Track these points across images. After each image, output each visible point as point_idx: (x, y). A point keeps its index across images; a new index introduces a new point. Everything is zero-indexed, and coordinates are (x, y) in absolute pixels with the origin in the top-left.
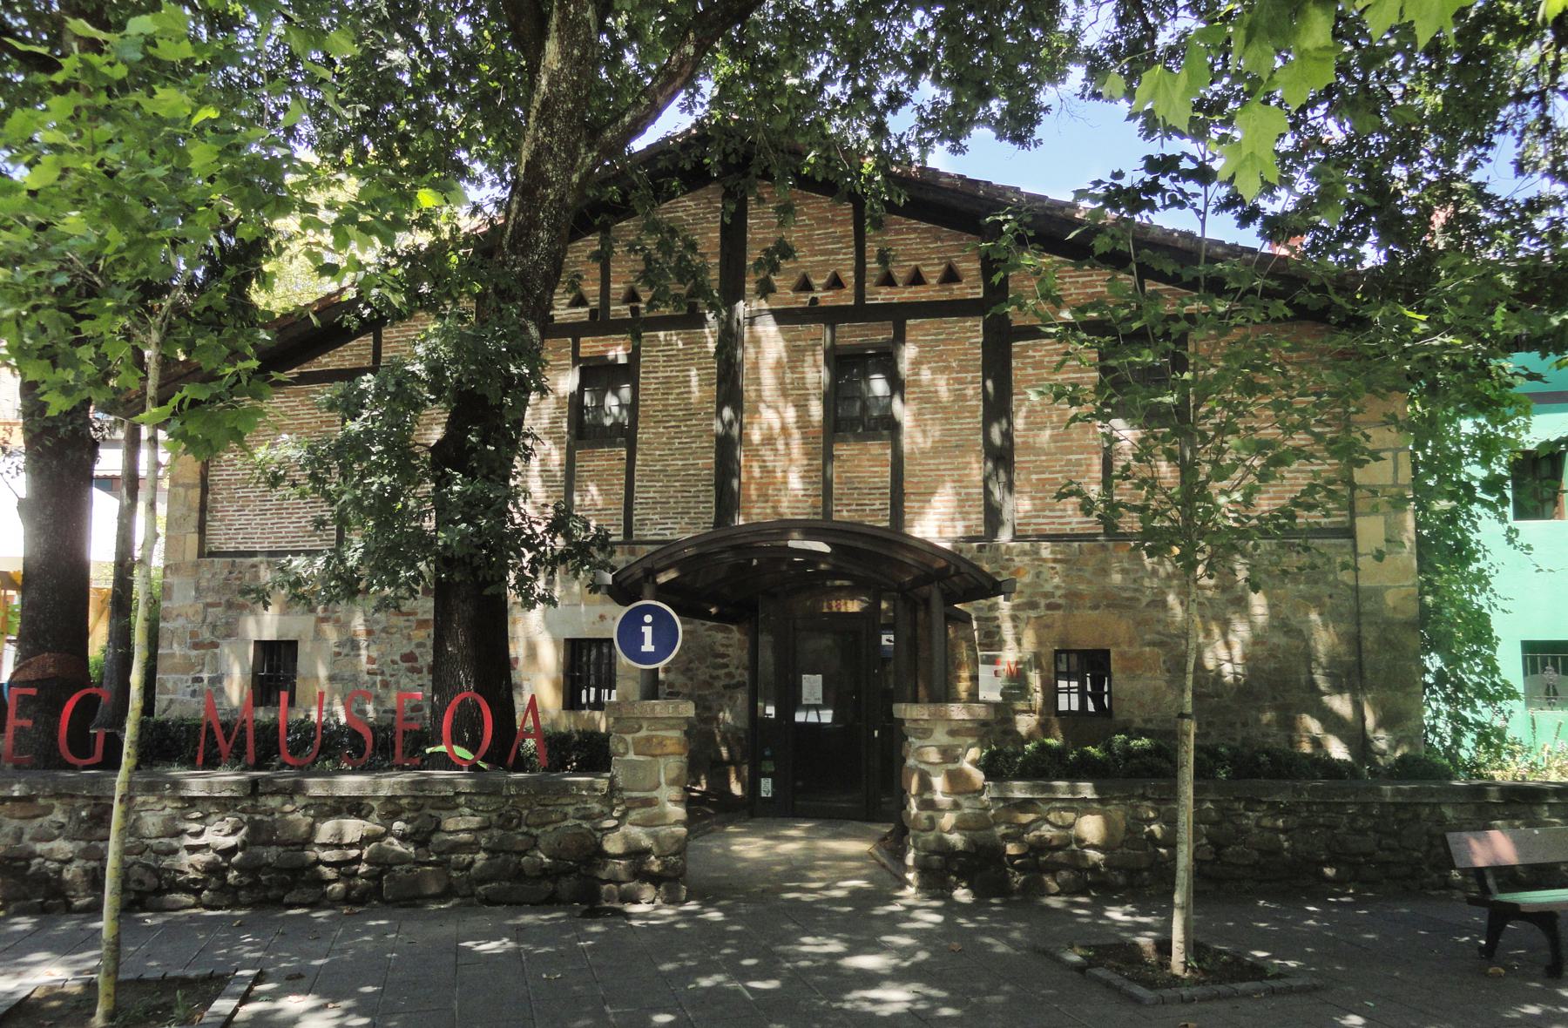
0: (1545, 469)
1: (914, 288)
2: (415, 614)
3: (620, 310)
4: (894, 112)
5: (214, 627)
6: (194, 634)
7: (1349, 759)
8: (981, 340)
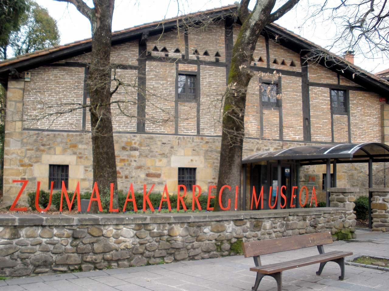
0: (193, 171)
3: (192, 57)
5: (30, 158)
6: (21, 161)
8: (301, 84)
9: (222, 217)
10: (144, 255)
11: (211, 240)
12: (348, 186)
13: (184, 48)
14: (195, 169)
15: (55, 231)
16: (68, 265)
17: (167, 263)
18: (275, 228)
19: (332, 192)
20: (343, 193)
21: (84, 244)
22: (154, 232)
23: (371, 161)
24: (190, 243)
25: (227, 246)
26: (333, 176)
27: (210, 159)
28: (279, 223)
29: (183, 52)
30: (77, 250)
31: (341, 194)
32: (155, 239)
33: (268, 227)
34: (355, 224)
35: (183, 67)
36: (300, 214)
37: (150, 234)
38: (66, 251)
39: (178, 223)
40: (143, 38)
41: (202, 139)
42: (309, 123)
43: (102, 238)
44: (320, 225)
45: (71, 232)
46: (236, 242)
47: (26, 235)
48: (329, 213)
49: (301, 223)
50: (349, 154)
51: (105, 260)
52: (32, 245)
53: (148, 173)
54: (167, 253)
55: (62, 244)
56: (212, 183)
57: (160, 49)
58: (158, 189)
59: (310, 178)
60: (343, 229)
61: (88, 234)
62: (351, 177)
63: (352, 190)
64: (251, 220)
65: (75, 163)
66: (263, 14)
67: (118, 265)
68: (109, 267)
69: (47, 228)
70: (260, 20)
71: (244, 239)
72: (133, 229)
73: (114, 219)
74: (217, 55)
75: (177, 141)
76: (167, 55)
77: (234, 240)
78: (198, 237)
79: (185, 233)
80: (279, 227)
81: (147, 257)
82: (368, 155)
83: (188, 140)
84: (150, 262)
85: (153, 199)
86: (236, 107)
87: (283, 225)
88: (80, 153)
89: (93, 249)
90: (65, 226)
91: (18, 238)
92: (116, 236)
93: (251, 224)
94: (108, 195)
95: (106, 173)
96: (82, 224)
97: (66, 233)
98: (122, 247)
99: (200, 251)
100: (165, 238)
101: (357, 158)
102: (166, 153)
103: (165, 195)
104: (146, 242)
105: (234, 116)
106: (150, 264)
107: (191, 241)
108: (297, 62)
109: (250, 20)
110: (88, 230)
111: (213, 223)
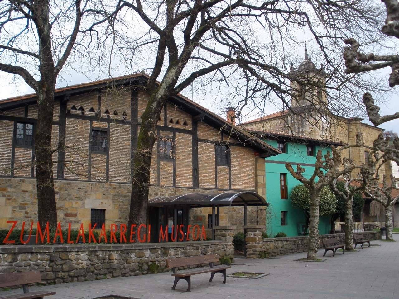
1: (177, 125)
2: (31, 217)
3: (105, 116)
4: (173, 79)
7: (201, 12)
9: (143, 246)
10: (94, 272)
11: (135, 263)
12: (228, 225)
13: (97, 107)
14: (104, 210)
15: (39, 256)
16: (47, 280)
17: (108, 278)
18: (177, 255)
19: (217, 229)
20: (225, 230)
21: (57, 265)
22: (100, 257)
23: (246, 205)
24: (122, 264)
25: (146, 267)
26: (217, 216)
27: (117, 202)
28: (180, 252)
29: (97, 112)
30: (52, 269)
31: (223, 231)
32: (100, 261)
33: (172, 255)
34: (233, 253)
35: (96, 124)
36: (194, 245)
37: (97, 258)
38: (46, 270)
39: (115, 250)
40: (65, 99)
41: (111, 185)
42: (198, 173)
43: (68, 261)
44: (209, 253)
45: (48, 257)
46: (151, 265)
47: (21, 259)
48: (215, 245)
49: (195, 251)
50: (229, 201)
51: (70, 276)
52: (24, 266)
53: (66, 213)
54: (108, 272)
55: (43, 265)
56: (119, 222)
57: (78, 108)
58: (75, 227)
59: (198, 218)
60: (225, 256)
61: (59, 258)
62: (231, 217)
63: (232, 227)
64: (161, 249)
65: (4, 204)
66: (167, 90)
67: (78, 279)
68: (72, 281)
69: (35, 254)
70: (165, 95)
71: (157, 263)
72: (87, 255)
73: (76, 247)
74: (125, 114)
75: (91, 187)
76: (83, 113)
77: (150, 263)
78: (127, 260)
79: (119, 258)
80: (180, 254)
81: (96, 274)
82: (244, 201)
83: (99, 186)
84: (98, 278)
85: (74, 235)
86: (145, 164)
87: (182, 252)
88: (9, 196)
89: (62, 269)
90: (46, 252)
91: (16, 261)
92: (77, 260)
93: (161, 252)
94: (52, 232)
95: (50, 214)
96: (56, 251)
97: (46, 257)
98: (80, 267)
99: (129, 271)
100: (107, 261)
101: (235, 203)
102: (81, 197)
103: (81, 232)
104: (95, 263)
105: (146, 172)
106: (98, 279)
107: (123, 263)
108: (189, 122)
109: (157, 94)
110: (59, 256)
111: (137, 251)
